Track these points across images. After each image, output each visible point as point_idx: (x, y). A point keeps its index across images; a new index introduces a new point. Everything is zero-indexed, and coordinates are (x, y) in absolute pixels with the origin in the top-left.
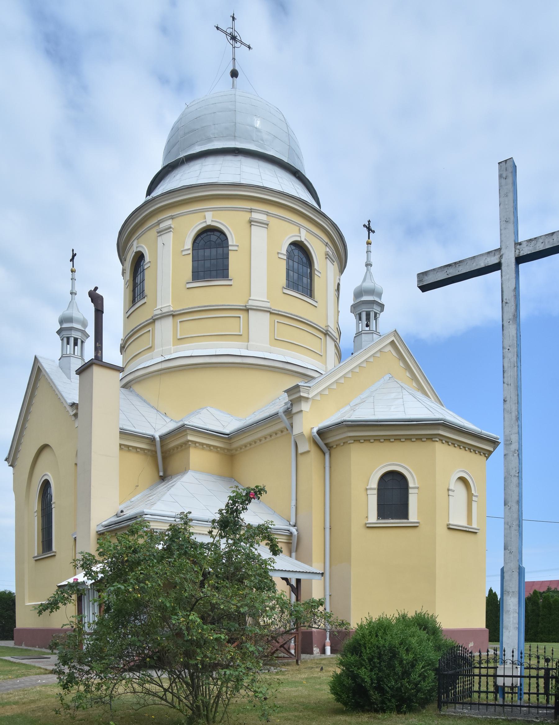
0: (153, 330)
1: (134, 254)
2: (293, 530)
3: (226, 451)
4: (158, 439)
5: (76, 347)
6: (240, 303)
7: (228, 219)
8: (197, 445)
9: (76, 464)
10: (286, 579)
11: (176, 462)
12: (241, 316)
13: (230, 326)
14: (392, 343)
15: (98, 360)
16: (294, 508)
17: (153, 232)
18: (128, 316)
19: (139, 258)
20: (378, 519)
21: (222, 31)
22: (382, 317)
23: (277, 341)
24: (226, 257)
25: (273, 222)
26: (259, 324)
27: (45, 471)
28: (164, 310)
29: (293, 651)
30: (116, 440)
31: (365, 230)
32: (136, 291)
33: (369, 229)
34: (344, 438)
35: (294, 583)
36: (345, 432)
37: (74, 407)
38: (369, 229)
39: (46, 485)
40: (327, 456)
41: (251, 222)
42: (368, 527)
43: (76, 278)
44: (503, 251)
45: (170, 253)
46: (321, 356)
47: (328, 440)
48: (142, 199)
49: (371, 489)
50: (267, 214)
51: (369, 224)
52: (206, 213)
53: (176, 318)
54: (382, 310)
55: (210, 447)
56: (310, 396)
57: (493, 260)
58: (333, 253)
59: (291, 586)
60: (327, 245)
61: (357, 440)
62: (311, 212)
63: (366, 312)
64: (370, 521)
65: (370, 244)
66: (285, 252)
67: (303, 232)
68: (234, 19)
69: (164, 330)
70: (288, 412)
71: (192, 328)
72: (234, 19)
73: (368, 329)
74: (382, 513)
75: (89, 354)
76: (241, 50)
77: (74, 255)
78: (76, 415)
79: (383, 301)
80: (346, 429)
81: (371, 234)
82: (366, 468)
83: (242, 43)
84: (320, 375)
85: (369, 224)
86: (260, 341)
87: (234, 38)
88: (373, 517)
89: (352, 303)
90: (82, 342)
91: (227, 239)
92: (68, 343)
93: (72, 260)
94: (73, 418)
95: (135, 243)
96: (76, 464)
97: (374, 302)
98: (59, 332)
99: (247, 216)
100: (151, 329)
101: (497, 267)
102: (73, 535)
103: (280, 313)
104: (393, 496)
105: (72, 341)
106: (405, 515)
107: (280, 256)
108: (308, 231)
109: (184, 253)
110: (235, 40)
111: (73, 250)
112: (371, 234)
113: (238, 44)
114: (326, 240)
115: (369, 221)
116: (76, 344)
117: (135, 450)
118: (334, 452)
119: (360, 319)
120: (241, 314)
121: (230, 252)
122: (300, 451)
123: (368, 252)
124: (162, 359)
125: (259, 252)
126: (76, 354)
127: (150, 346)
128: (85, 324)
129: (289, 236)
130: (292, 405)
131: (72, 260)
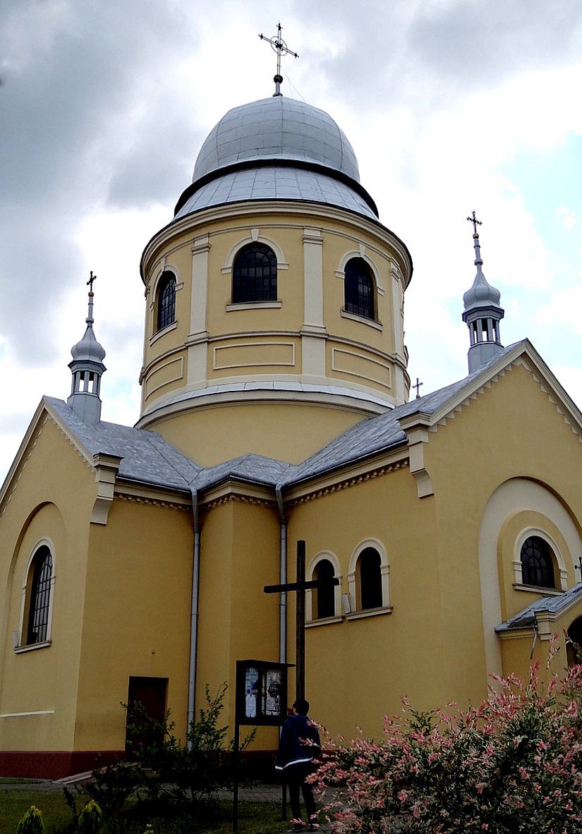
0: (186, 359)
1: (161, 273)
3: (266, 503)
4: (194, 493)
8: (251, 500)
13: (275, 353)
14: (524, 355)
17: (188, 249)
18: (150, 344)
19: (168, 277)
22: (502, 324)
24: (274, 276)
25: (327, 237)
26: (314, 352)
39: (43, 553)
41: (305, 239)
45: (205, 278)
50: (321, 230)
53: (211, 345)
55: (256, 501)
62: (369, 225)
66: (343, 271)
67: (362, 248)
68: (280, 28)
69: (198, 359)
71: (231, 356)
72: (280, 28)
76: (287, 59)
77: (92, 280)
79: (502, 305)
84: (389, 410)
86: (314, 373)
87: (279, 46)
89: (463, 310)
90: (99, 377)
98: (70, 366)
99: (298, 233)
105: (87, 375)
107: (337, 275)
108: (368, 247)
111: (92, 272)
113: (283, 53)
115: (474, 212)
119: (475, 329)
120: (293, 342)
121: (278, 271)
123: (477, 246)
125: (311, 274)
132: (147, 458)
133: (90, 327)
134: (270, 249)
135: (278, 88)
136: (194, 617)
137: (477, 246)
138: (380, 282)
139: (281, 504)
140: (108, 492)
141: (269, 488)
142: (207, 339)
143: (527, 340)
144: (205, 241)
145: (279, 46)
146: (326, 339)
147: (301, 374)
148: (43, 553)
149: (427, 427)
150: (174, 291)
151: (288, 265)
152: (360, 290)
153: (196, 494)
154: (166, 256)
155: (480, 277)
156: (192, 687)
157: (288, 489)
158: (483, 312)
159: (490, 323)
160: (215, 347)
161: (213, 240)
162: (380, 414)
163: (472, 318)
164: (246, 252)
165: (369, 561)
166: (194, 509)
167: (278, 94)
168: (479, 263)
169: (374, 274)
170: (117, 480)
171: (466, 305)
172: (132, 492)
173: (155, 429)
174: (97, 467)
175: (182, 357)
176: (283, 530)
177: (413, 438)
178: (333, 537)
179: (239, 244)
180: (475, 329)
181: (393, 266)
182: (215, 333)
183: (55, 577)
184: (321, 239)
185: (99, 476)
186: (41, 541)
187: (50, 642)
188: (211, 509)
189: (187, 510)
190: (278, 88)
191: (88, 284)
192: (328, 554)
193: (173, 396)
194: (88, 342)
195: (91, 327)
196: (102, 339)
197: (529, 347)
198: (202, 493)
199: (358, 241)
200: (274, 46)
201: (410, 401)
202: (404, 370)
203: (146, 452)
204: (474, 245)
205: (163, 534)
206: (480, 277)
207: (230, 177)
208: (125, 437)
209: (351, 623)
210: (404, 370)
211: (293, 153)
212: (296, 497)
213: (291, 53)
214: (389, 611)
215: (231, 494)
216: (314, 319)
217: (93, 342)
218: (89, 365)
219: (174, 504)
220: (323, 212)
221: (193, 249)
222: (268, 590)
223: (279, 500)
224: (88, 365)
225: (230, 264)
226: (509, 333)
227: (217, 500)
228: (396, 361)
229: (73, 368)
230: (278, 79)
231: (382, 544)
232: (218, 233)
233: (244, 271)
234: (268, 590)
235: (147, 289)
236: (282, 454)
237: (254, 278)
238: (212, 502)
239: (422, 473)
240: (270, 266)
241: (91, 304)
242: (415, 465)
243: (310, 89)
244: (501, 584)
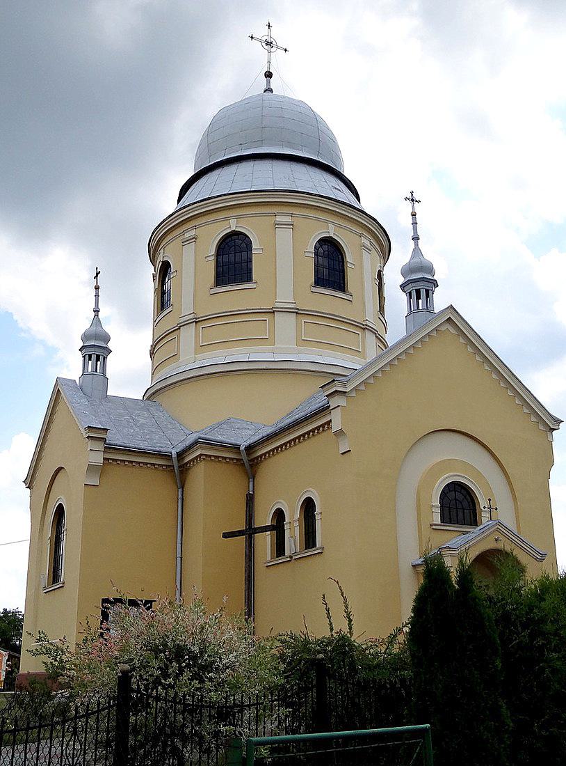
6: (267, 306)
17: (178, 241)
18: (156, 325)
24: (250, 260)
25: (296, 221)
26: (285, 325)
31: (416, 197)
39: (60, 511)
45: (195, 261)
63: (416, 290)
67: (331, 227)
68: (269, 26)
69: (188, 334)
72: (269, 26)
77: (98, 274)
86: (286, 344)
88: (437, 518)
90: (105, 359)
92: (90, 359)
97: (423, 279)
98: (403, 287)
105: (94, 357)
114: (360, 231)
116: (98, 359)
125: (283, 257)
126: (98, 371)
132: (142, 426)
133: (96, 315)
134: (247, 236)
135: (268, 83)
136: (179, 559)
138: (349, 258)
139: (249, 461)
140: (98, 459)
141: (236, 448)
143: (451, 306)
144: (192, 233)
145: (269, 44)
152: (331, 268)
154: (164, 248)
155: (417, 251)
157: (250, 448)
158: (420, 284)
161: (198, 232)
163: (409, 288)
164: (228, 240)
165: (309, 505)
166: (177, 468)
167: (269, 90)
170: (105, 447)
172: (118, 457)
173: (157, 399)
174: (88, 437)
176: (251, 484)
177: (334, 402)
178: (280, 491)
181: (364, 240)
183: (66, 529)
184: (291, 223)
185: (91, 445)
189: (170, 468)
190: (268, 83)
192: (281, 503)
193: (170, 370)
196: (108, 328)
197: (455, 314)
198: (180, 455)
200: (264, 45)
203: (142, 421)
205: (152, 490)
206: (417, 251)
207: (216, 172)
208: (126, 408)
211: (271, 145)
213: (281, 48)
214: (320, 551)
215: (201, 455)
216: (285, 297)
218: (96, 349)
219: (159, 465)
220: (278, 198)
221: (183, 241)
222: (226, 535)
223: (244, 457)
224: (96, 349)
225: (213, 252)
226: (440, 300)
228: (365, 327)
230: (269, 75)
231: (284, 502)
232: (202, 225)
234: (226, 535)
236: (247, 416)
237: (234, 261)
238: (189, 462)
239: (340, 433)
241: (97, 296)
242: (335, 426)
244: (419, 521)
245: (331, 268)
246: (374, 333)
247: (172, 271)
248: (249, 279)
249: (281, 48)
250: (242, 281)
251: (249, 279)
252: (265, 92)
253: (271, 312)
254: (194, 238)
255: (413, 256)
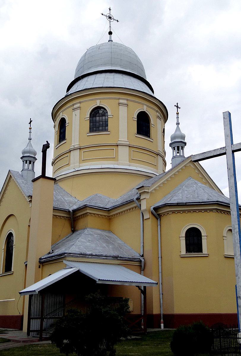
1: (60, 118)
2: (141, 258)
5: (30, 165)
6: (114, 143)
7: (107, 103)
9: (29, 226)
10: (138, 287)
11: (81, 223)
12: (114, 149)
15: (43, 176)
16: (142, 247)
17: (71, 109)
19: (63, 121)
20: (186, 252)
21: (105, 15)
22: (186, 148)
23: (132, 160)
25: (130, 104)
26: (123, 152)
27: (10, 228)
28: (76, 146)
29: (143, 327)
30: (51, 213)
32: (62, 136)
33: (177, 107)
34: (167, 212)
35: (142, 289)
36: (168, 209)
37: (30, 197)
38: (177, 107)
39: (10, 235)
40: (159, 221)
42: (181, 257)
43: (31, 132)
44: (227, 148)
45: (78, 120)
46: (155, 166)
47: (158, 213)
48: (64, 94)
49: (182, 237)
50: (127, 100)
51: (177, 105)
52: (97, 101)
53: (81, 150)
54: (185, 145)
56: (149, 191)
57: (223, 151)
58: (160, 115)
59: (141, 290)
60: (157, 111)
61: (173, 212)
64: (182, 254)
65: (178, 114)
66: (136, 118)
68: (110, 9)
69: (75, 155)
70: (138, 199)
72: (110, 9)
73: (178, 154)
74: (188, 250)
75: (38, 172)
76: (114, 23)
77: (31, 121)
78: (30, 201)
79: (186, 141)
80: (168, 207)
81: (179, 109)
82: (177, 228)
83: (114, 19)
84: (155, 176)
85: (177, 105)
86: (123, 161)
87: (110, 18)
90: (34, 163)
91: (107, 112)
92: (26, 163)
93: (30, 123)
94: (29, 202)
95: (61, 114)
96: (29, 226)
97: (181, 142)
98: (22, 158)
99: (117, 101)
100: (68, 155)
101: (225, 154)
102: (25, 263)
103: (134, 146)
104: (194, 241)
105: (28, 162)
106: (200, 250)
109: (133, 119)
110: (111, 19)
111: (31, 119)
112: (179, 109)
114: (157, 109)
115: (177, 103)
116: (30, 163)
117: (59, 217)
118: (162, 218)
119: (174, 150)
120: (114, 148)
122: (145, 218)
123: (178, 118)
124: (73, 170)
127: (68, 163)
128: (35, 154)
129: (139, 109)
130: (140, 195)
131: (30, 123)
135: (110, 37)
137: (178, 118)
138: (152, 122)
142: (79, 148)
144: (78, 105)
146: (129, 146)
147: (118, 161)
148: (10, 235)
149: (148, 192)
150: (65, 127)
151: (113, 116)
152: (143, 125)
153: (72, 212)
155: (178, 129)
156: (160, 267)
159: (180, 148)
160: (83, 151)
161: (81, 105)
162: (152, 177)
163: (173, 146)
168: (178, 124)
169: (149, 117)
171: (172, 139)
175: (68, 155)
179: (89, 111)
180: (174, 150)
182: (83, 145)
186: (9, 230)
187: (13, 272)
188: (79, 219)
190: (110, 37)
191: (29, 124)
194: (28, 148)
195: (30, 142)
199: (143, 104)
200: (112, 17)
201: (166, 171)
202: (163, 158)
204: (176, 117)
206: (178, 129)
209: (183, 258)
210: (163, 158)
212: (111, 215)
217: (31, 148)
227: (81, 215)
229: (23, 159)
233: (94, 118)
235: (55, 125)
237: (98, 120)
238: (79, 216)
240: (105, 116)
243: (123, 36)
245: (143, 125)
246: (162, 157)
247: (67, 123)
248: (106, 130)
249: (105, 15)
250: (102, 131)
251: (106, 130)
252: (109, 41)
253: (116, 145)
254: (79, 107)
255: (176, 131)
